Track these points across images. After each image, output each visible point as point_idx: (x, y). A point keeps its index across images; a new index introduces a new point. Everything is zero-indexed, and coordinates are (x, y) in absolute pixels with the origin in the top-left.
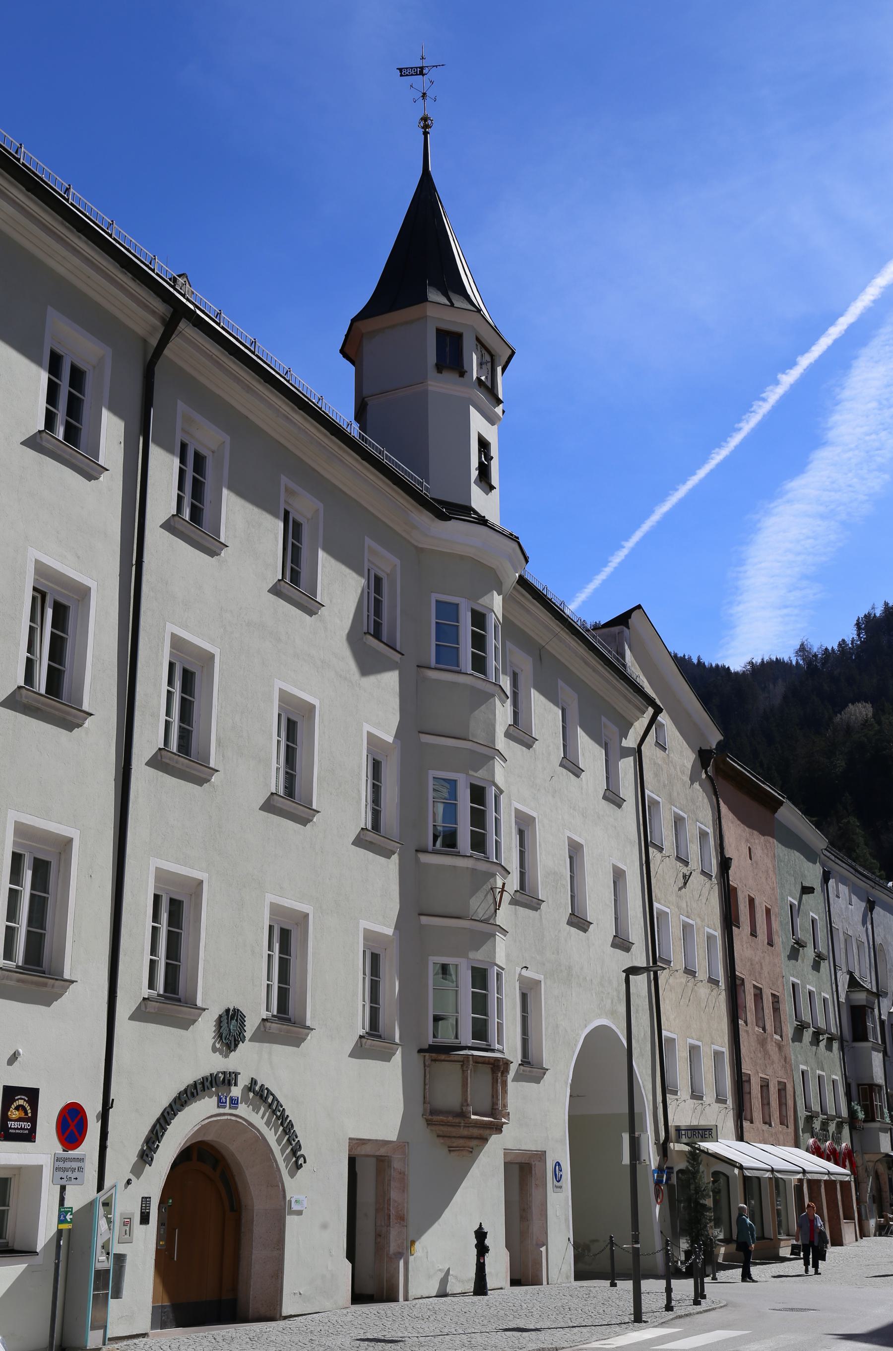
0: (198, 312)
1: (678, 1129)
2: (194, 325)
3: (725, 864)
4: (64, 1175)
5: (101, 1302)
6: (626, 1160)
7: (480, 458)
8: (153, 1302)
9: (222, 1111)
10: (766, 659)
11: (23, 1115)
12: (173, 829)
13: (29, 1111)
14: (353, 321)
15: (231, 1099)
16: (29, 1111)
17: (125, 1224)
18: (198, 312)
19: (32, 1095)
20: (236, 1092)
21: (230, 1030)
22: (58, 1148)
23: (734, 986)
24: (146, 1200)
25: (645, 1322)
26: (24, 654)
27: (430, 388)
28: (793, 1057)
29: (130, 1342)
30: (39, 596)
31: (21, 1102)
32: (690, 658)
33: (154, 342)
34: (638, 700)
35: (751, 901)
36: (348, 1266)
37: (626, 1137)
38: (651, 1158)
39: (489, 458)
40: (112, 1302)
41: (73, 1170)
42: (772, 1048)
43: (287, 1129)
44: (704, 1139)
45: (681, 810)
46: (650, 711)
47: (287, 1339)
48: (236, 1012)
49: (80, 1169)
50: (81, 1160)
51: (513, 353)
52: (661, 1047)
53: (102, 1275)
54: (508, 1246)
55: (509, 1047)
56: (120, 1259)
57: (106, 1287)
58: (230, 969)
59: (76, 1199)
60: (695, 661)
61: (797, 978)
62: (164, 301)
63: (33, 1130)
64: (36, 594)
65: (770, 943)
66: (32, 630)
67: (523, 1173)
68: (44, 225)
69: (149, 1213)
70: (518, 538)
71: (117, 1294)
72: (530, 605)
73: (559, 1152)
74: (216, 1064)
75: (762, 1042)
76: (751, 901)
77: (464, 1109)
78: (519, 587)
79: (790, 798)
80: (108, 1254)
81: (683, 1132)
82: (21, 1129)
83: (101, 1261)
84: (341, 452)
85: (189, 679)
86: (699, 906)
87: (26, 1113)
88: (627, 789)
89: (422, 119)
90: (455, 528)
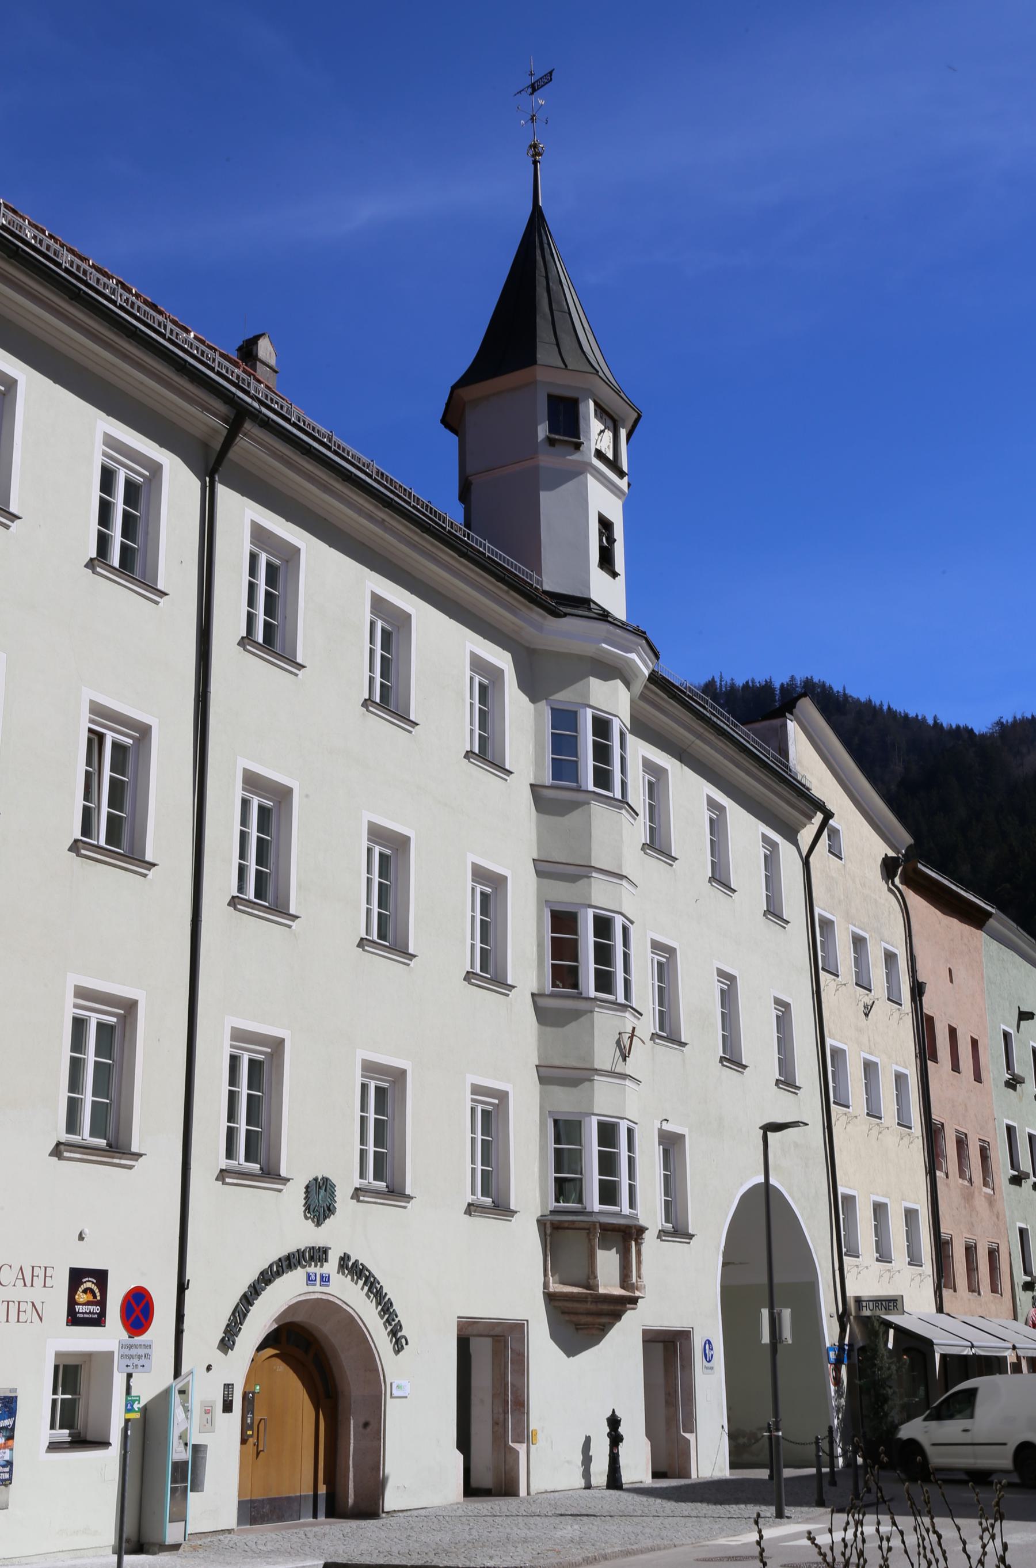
0: (264, 410)
1: (858, 1300)
2: (261, 426)
3: (918, 990)
4: (130, 1363)
5: (180, 1496)
6: (766, 1339)
7: (601, 540)
8: (240, 1495)
9: (311, 1288)
10: (1019, 717)
11: (91, 1298)
12: (255, 978)
13: (98, 1294)
14: (454, 388)
15: (322, 1276)
16: (98, 1294)
17: (207, 1412)
18: (264, 410)
19: (101, 1277)
20: (331, 1266)
21: (319, 1201)
22: (124, 1335)
23: (932, 1133)
24: (228, 1387)
25: (788, 1517)
26: (79, 802)
27: (542, 464)
28: (1007, 1213)
29: (215, 1538)
30: (96, 738)
31: (89, 1285)
32: (924, 719)
33: (217, 445)
34: (802, 804)
35: (953, 1032)
36: (460, 1457)
37: (765, 1313)
38: (830, 1333)
39: (611, 540)
40: (191, 1495)
41: (140, 1357)
42: (980, 1203)
43: (387, 1309)
44: (888, 1310)
45: (861, 929)
46: (819, 817)
47: (383, 1535)
48: (326, 1180)
49: (147, 1356)
50: (148, 1346)
51: (639, 416)
52: (840, 1207)
53: (180, 1468)
54: (650, 1434)
55: (649, 1211)
56: (198, 1450)
57: (185, 1480)
58: (317, 1131)
59: (146, 1389)
60: (931, 722)
61: (1013, 1119)
62: (226, 403)
63: (103, 1314)
64: (92, 736)
65: (978, 1078)
66: (88, 775)
67: (667, 1350)
68: (87, 330)
69: (232, 1401)
70: (644, 633)
71: (197, 1486)
72: (667, 706)
73: (707, 1326)
74: (305, 1234)
75: (968, 1197)
76: (953, 1032)
77: (591, 1282)
78: (652, 687)
79: (1001, 908)
80: (186, 1444)
81: (864, 1304)
82: (90, 1313)
83: (178, 1453)
84: (434, 550)
85: (269, 812)
86: (891, 1041)
87: (95, 1296)
88: (793, 905)
89: (530, 146)
90: (570, 625)
